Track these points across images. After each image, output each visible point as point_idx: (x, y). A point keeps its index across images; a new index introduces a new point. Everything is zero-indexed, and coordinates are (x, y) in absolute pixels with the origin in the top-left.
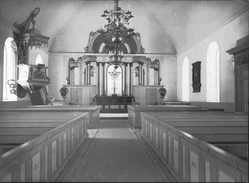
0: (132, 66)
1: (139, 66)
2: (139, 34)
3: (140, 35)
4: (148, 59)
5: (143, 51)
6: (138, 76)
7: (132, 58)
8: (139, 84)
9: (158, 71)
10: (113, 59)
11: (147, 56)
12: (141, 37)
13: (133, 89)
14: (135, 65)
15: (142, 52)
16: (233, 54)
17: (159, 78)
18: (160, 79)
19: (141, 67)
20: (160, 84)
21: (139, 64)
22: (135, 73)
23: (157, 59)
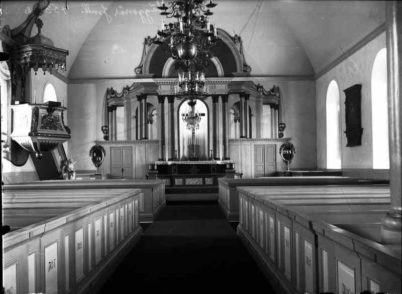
1: (241, 100)
2: (239, 38)
3: (242, 39)
7: (227, 85)
8: (241, 137)
11: (256, 81)
14: (233, 99)
18: (283, 126)
20: (283, 136)
21: (241, 96)
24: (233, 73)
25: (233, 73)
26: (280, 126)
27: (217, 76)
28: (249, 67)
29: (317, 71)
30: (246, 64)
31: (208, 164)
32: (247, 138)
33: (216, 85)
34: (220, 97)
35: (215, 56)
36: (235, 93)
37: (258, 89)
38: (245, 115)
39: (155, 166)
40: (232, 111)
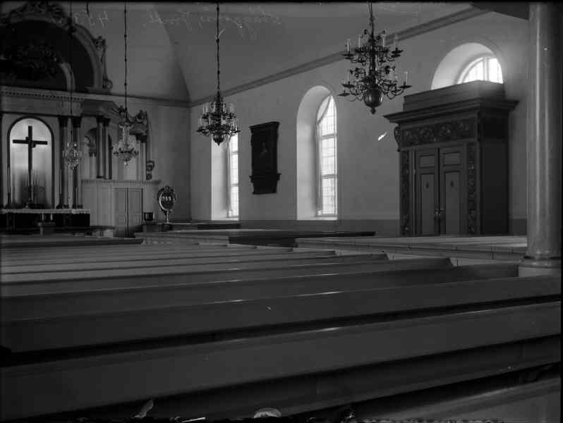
0: (80, 127)
1: (98, 125)
2: (104, 42)
3: (107, 43)
4: (122, 111)
5: (108, 86)
6: (95, 155)
7: (79, 104)
8: (98, 177)
9: (146, 143)
10: (211, 122)
11: (119, 101)
12: (107, 50)
13: (82, 187)
14: (88, 123)
15: (104, 90)
16: (397, 122)
17: (150, 162)
18: (151, 164)
19: (104, 131)
20: (151, 177)
21: (98, 121)
22: (89, 145)
23: (144, 111)
24: (88, 88)
25: (88, 88)
26: (148, 164)
27: (65, 90)
28: (111, 82)
29: (194, 97)
30: (107, 77)
31: (60, 214)
32: (105, 179)
33: (65, 103)
34: (70, 119)
35: (66, 61)
36: (91, 116)
37: (120, 112)
38: (100, 143)
39: (51, 216)
40: (86, 141)
